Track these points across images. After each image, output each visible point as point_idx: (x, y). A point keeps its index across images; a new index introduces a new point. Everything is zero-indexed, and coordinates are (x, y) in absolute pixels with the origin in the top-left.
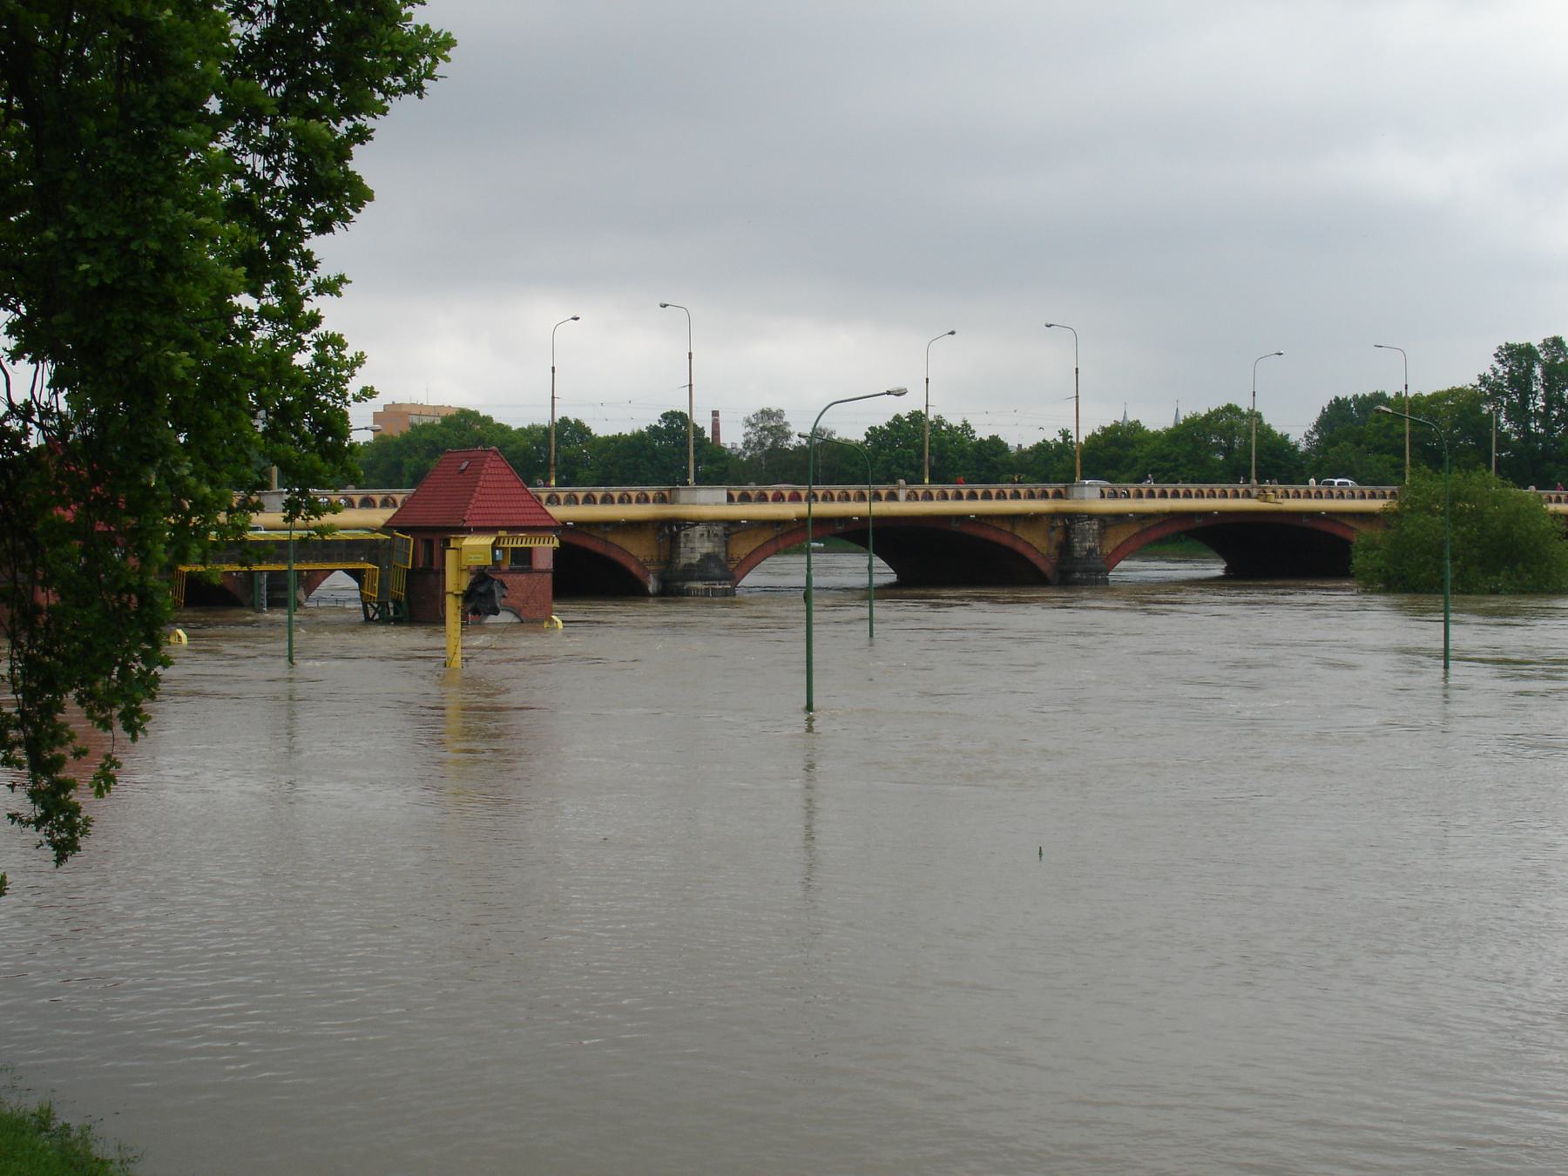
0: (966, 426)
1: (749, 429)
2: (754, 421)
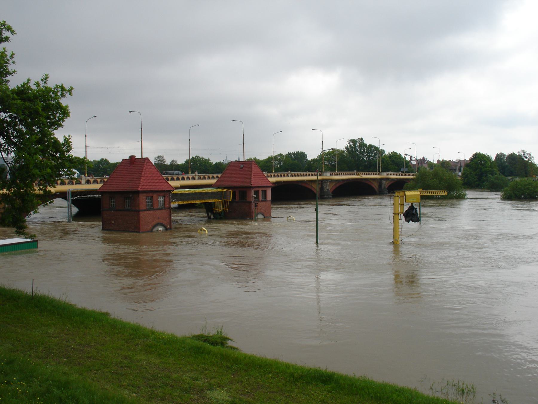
0: (208, 159)
1: (155, 160)
2: (157, 158)
